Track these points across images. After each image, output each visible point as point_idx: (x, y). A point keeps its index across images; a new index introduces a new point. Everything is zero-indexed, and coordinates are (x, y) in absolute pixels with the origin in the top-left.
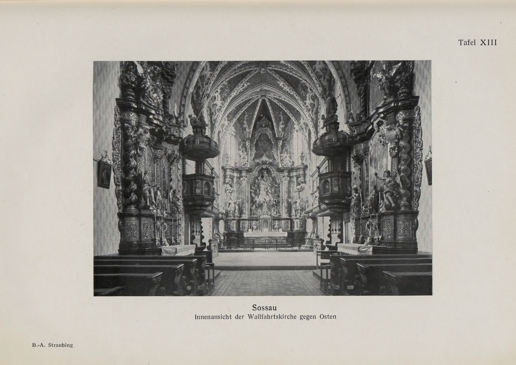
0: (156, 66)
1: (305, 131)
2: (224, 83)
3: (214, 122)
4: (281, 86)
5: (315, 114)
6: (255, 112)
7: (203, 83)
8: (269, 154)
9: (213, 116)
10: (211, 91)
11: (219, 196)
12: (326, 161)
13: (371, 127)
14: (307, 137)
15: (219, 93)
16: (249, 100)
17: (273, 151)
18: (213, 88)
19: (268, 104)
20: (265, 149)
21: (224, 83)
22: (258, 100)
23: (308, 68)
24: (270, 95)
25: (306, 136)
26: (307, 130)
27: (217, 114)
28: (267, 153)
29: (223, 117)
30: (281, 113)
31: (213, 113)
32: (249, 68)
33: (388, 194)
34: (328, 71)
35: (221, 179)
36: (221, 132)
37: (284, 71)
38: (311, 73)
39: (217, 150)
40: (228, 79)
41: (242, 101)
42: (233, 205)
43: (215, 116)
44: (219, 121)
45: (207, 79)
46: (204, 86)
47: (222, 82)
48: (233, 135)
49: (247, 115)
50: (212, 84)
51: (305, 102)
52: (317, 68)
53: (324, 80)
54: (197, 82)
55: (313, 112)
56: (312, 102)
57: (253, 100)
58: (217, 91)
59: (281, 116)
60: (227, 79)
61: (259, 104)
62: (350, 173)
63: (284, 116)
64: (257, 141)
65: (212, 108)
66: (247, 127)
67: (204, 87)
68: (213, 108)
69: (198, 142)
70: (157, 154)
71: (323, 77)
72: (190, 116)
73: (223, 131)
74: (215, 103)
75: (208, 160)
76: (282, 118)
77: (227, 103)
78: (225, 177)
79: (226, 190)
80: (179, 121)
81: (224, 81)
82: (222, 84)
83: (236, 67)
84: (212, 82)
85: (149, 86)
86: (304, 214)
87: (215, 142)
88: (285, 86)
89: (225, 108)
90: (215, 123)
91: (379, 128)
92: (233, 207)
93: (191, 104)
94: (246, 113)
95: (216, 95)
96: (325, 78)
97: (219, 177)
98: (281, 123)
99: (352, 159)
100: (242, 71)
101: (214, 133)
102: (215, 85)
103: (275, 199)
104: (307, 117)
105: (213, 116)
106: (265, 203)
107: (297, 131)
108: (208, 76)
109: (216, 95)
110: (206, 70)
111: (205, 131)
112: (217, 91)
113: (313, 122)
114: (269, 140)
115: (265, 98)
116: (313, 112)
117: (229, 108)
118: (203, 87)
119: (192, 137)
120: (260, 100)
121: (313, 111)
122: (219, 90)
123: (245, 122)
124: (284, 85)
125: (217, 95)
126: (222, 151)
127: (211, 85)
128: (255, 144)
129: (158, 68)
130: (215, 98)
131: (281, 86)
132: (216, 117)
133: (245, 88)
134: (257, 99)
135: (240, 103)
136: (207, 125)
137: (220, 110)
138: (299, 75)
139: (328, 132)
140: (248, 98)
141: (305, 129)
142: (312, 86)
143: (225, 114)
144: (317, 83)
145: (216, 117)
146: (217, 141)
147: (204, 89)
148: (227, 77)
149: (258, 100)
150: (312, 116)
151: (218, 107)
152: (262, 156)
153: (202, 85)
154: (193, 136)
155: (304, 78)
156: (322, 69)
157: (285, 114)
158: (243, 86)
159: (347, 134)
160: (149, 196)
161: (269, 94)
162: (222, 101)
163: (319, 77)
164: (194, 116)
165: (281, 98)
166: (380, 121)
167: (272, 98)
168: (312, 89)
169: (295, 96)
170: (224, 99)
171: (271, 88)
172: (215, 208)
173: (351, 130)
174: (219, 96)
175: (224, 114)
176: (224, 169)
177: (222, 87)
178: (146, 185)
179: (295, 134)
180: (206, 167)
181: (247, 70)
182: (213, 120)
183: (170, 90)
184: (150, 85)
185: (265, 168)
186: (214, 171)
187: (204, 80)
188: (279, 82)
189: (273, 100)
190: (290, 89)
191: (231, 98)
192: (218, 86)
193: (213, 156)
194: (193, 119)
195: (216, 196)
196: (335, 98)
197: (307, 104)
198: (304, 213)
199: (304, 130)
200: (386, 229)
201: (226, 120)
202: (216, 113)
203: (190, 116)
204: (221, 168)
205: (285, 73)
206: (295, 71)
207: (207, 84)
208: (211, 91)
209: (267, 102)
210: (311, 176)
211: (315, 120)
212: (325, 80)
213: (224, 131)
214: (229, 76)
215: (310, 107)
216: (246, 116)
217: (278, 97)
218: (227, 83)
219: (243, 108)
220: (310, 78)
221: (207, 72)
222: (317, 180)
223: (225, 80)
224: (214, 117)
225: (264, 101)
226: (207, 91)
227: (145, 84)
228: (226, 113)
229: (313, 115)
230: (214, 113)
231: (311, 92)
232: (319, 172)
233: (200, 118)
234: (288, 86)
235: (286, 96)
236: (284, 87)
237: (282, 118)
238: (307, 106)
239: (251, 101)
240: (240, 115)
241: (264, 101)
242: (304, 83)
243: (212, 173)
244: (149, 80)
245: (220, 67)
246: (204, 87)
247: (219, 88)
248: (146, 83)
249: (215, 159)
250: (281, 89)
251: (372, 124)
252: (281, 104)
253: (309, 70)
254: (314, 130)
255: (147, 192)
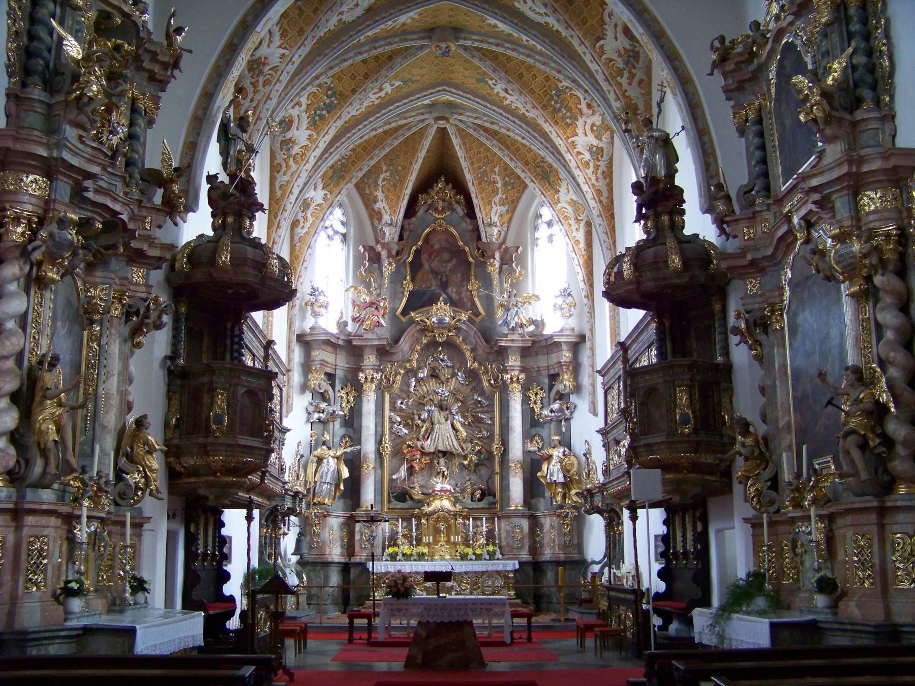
0: (120, 41)
1: (574, 227)
2: (323, 79)
3: (279, 193)
4: (498, 93)
5: (605, 178)
6: (411, 163)
7: (257, 81)
8: (459, 293)
9: (278, 175)
10: (279, 103)
11: (287, 435)
12: (648, 324)
13: (784, 229)
14: (582, 245)
15: (304, 107)
16: (396, 129)
17: (470, 287)
18: (286, 95)
19: (456, 141)
20: (444, 280)
21: (323, 79)
22: (425, 129)
23: (580, 49)
24: (461, 118)
25: (577, 242)
26: (582, 224)
27: (294, 167)
28: (449, 290)
29: (311, 177)
30: (497, 170)
31: (280, 165)
32: (401, 41)
33: (851, 439)
34: (641, 59)
35: (296, 377)
36: (302, 224)
37: (509, 53)
38: (591, 62)
39: (288, 285)
40: (336, 70)
41: (374, 133)
42: (333, 463)
43: (285, 173)
44: (296, 191)
45: (270, 69)
46: (260, 87)
47: (317, 77)
48: (336, 232)
49: (388, 174)
50: (283, 84)
51: (573, 142)
52: (607, 48)
53: (630, 84)
54: (241, 78)
55: (599, 172)
56: (595, 142)
57: (409, 129)
58: (298, 104)
59: (496, 177)
60: (331, 68)
61: (426, 143)
62: (728, 368)
63: (507, 179)
64: (418, 253)
65: (279, 150)
66: (387, 208)
67: (258, 91)
68: (281, 150)
69: (225, 258)
70: (94, 297)
71: (626, 75)
72: (211, 179)
73: (306, 219)
74: (289, 135)
75: (253, 314)
76: (499, 185)
77: (328, 138)
78: (307, 367)
79: (309, 414)
80: (173, 192)
81: (321, 74)
82: (318, 82)
83: (362, 38)
84: (285, 78)
85: (97, 96)
86: (575, 498)
87: (280, 259)
88: (511, 92)
89: (318, 152)
90: (283, 196)
91: (809, 233)
92: (332, 469)
93: (218, 141)
94: (384, 168)
95: (295, 112)
96: (632, 76)
97: (289, 371)
98: (497, 199)
99: (734, 339)
100: (380, 50)
101: (279, 227)
102: (292, 87)
103: (478, 448)
104: (579, 185)
105: (278, 175)
106: (120, 161)
107: (550, 224)
108: (274, 60)
109: (295, 112)
110: (269, 46)
111: (251, 225)
112: (298, 104)
113: (601, 202)
114: (459, 254)
115: (448, 126)
116: (599, 172)
117: (331, 150)
118: (256, 92)
119: (209, 242)
120: (432, 131)
121: (597, 167)
122: (304, 100)
123: (379, 194)
124: (506, 91)
125: (298, 113)
126: (303, 286)
127: (280, 87)
128: (411, 263)
129: (126, 46)
130: (291, 122)
131: (498, 93)
132: (286, 178)
133: (387, 94)
134: (421, 126)
135: (366, 137)
136: (260, 207)
137: (302, 157)
138: (553, 65)
139: (651, 237)
140: (393, 125)
141: (576, 219)
142: (593, 99)
143: (316, 171)
144: (609, 91)
145: (286, 178)
146: (286, 255)
147: (258, 97)
148: (332, 64)
149: (425, 129)
150: (596, 184)
151: (296, 150)
152: (432, 300)
153: (254, 85)
154: (210, 240)
155: (569, 75)
156: (623, 52)
157: (507, 171)
158: (381, 90)
159: (710, 244)
160: (55, 441)
161: (461, 114)
162: (309, 132)
163: (613, 76)
164: (224, 178)
165: (495, 127)
166: (811, 211)
167: (468, 126)
168: (594, 104)
169: (541, 121)
170: (316, 123)
171: (469, 96)
172: (272, 476)
173: (722, 231)
174: (304, 116)
175: (316, 167)
176: (304, 341)
177: (314, 89)
178: (49, 402)
179: (543, 232)
180: (248, 337)
181: (394, 47)
182: (277, 187)
183: (156, 100)
184: (99, 92)
185: (443, 340)
186: (275, 352)
187: (261, 72)
188: (490, 82)
189: (471, 131)
190: (526, 103)
191: (340, 123)
192: (304, 89)
193: (271, 305)
194: (221, 186)
195: (277, 434)
196: (668, 135)
197: (579, 148)
198: (577, 494)
199: (572, 222)
200: (856, 559)
201: (320, 186)
202: (288, 167)
203: (211, 179)
204: (294, 338)
205: (509, 58)
206: (541, 54)
207: (267, 83)
208: (279, 103)
209: (453, 138)
210: (599, 372)
211: (605, 194)
212: (634, 84)
213: (311, 220)
214: (337, 61)
215: (587, 156)
216: (382, 177)
217: (487, 125)
218: (331, 79)
219: (377, 152)
220: (587, 75)
221: (269, 50)
222: (619, 386)
223: (325, 73)
224: (282, 179)
225: (443, 132)
226: (269, 102)
227: (83, 89)
228: (319, 167)
229: (597, 180)
230: (284, 165)
231: (590, 112)
232: (625, 360)
233: (240, 185)
234: (521, 93)
235: (514, 122)
236: (507, 96)
237: (499, 185)
238: (579, 153)
239: (401, 132)
240: (363, 172)
241: (443, 132)
242: (567, 88)
243: (266, 357)
244: (97, 77)
245: (314, 37)
246: (258, 91)
247: (305, 94)
248: (86, 87)
249: (280, 314)
250: (497, 103)
251: (788, 218)
252: (495, 142)
253: (584, 53)
254: (605, 223)
255: (52, 427)
